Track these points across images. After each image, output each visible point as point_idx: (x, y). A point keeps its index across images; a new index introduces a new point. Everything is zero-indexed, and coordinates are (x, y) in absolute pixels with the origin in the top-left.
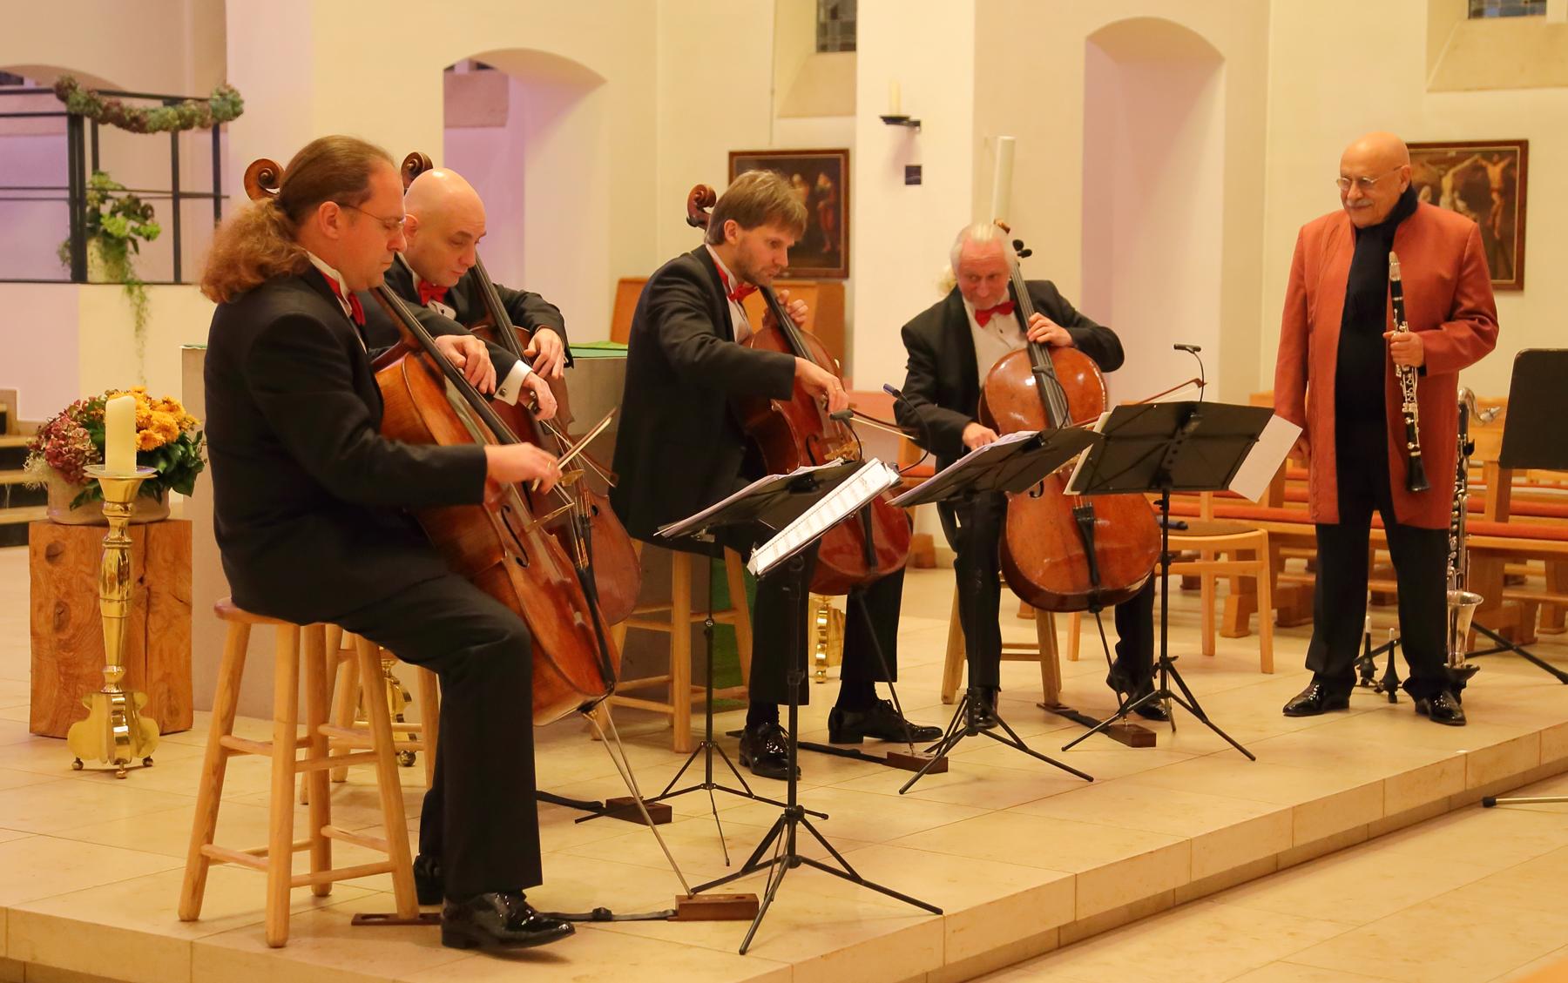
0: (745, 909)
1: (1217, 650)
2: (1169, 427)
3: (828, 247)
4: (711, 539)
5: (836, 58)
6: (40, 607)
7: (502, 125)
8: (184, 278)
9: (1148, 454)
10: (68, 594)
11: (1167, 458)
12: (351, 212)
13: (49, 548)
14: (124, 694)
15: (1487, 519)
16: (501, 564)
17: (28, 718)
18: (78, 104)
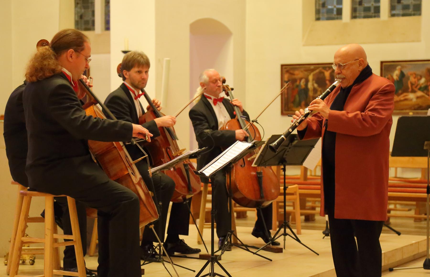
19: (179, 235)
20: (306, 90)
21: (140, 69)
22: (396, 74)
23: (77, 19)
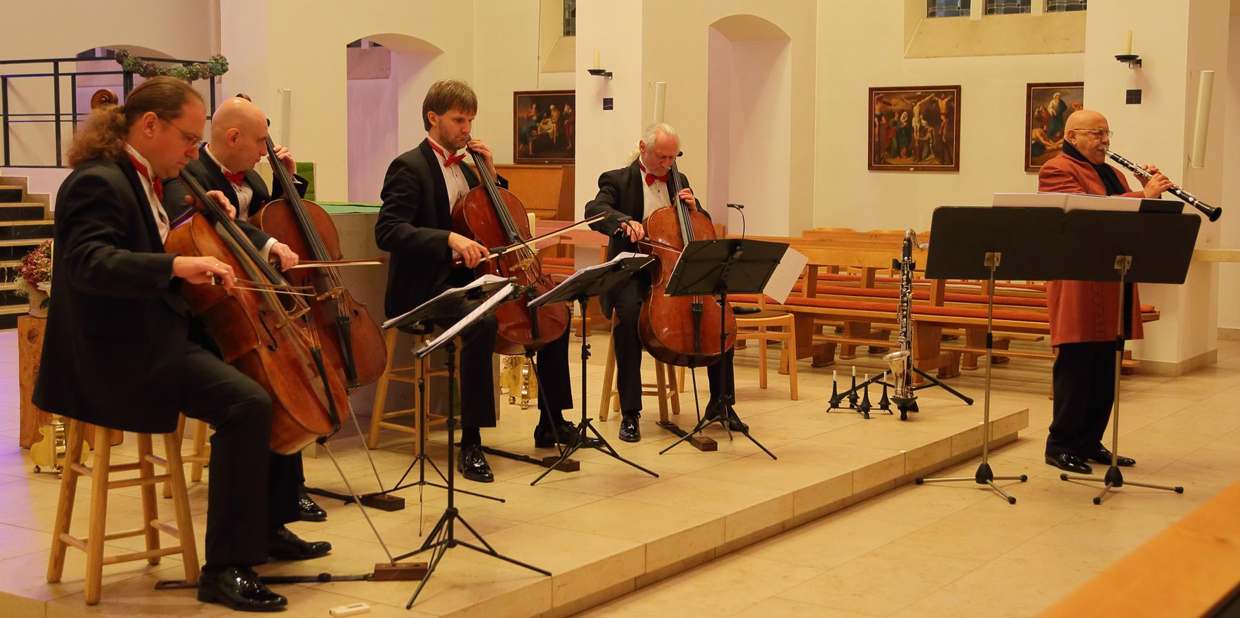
0: (419, 574)
2: (725, 254)
4: (422, 328)
5: (571, 38)
8: (63, 164)
13: (30, 332)
15: (931, 305)
17: (17, 434)
19: (563, 411)
20: (909, 128)
21: (463, 116)
22: (1052, 106)
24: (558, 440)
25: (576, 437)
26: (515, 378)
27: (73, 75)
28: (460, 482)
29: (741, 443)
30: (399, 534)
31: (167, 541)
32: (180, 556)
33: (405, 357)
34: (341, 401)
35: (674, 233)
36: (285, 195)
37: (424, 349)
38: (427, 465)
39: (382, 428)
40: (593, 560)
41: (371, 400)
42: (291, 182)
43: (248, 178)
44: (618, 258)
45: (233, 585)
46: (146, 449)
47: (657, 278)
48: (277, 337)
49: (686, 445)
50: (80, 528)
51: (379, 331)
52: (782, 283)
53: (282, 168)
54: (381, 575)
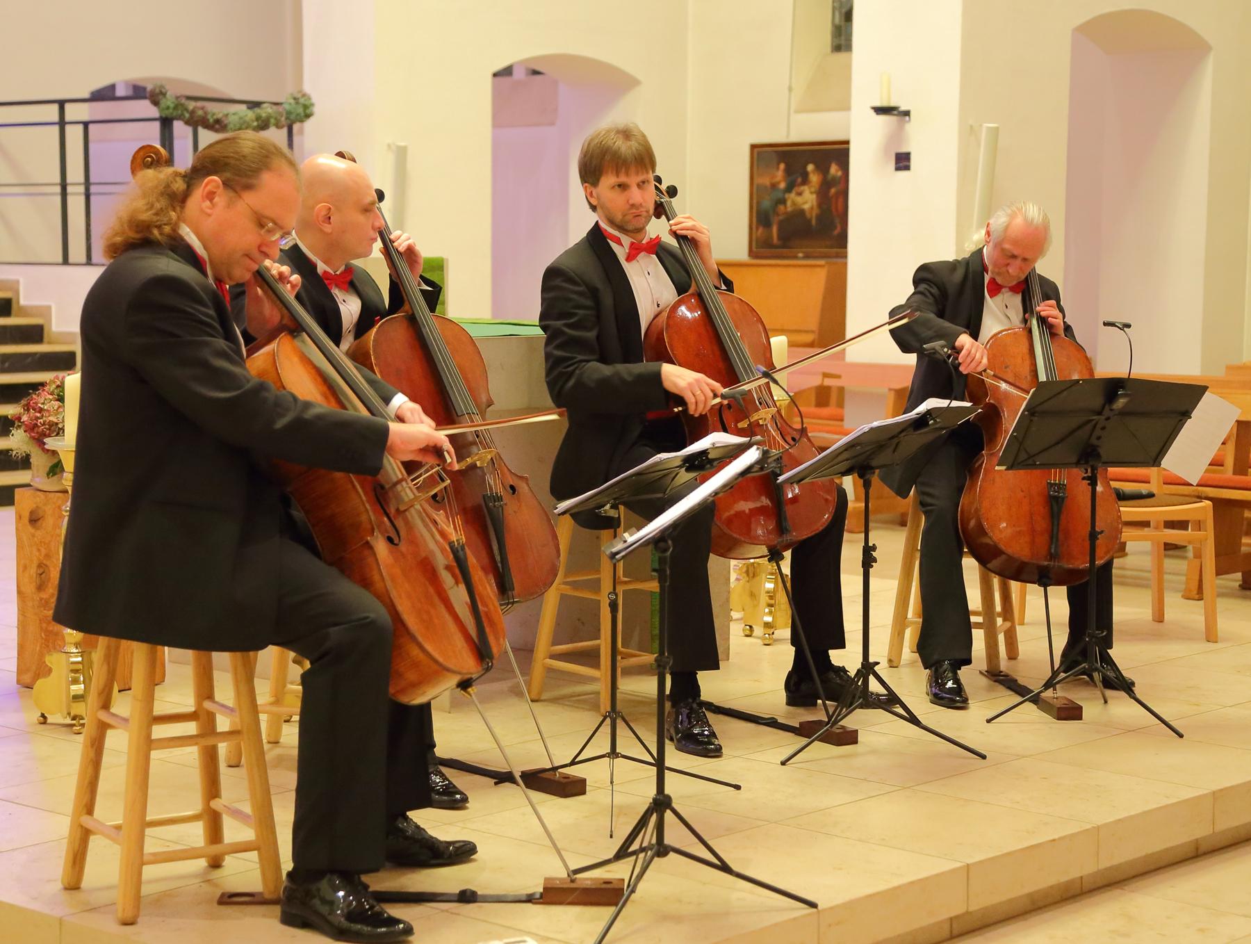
1: (1168, 615)
2: (1098, 401)
3: (836, 232)
5: (841, 56)
6: (25, 568)
7: (552, 124)
9: (1079, 428)
10: (47, 556)
11: (1094, 437)
12: (232, 194)
13: (32, 513)
14: (82, 654)
16: (367, 542)
17: (12, 666)
18: (168, 108)
19: (830, 652)
21: (623, 179)
23: (837, 21)
24: (823, 691)
25: (851, 692)
26: (753, 595)
27: (86, 125)
28: (674, 758)
29: (1121, 707)
30: (577, 833)
31: (234, 831)
32: (253, 855)
33: (586, 559)
34: (492, 624)
35: (1025, 370)
36: (406, 307)
37: (620, 546)
38: (622, 730)
39: (550, 670)
40: (882, 887)
41: (532, 625)
42: (414, 288)
43: (353, 281)
44: (922, 408)
45: (332, 903)
46: (205, 690)
47: (993, 438)
48: (400, 523)
49: (1029, 707)
50: (111, 809)
51: (542, 521)
52: (1195, 449)
53: (403, 266)
54: (553, 895)
